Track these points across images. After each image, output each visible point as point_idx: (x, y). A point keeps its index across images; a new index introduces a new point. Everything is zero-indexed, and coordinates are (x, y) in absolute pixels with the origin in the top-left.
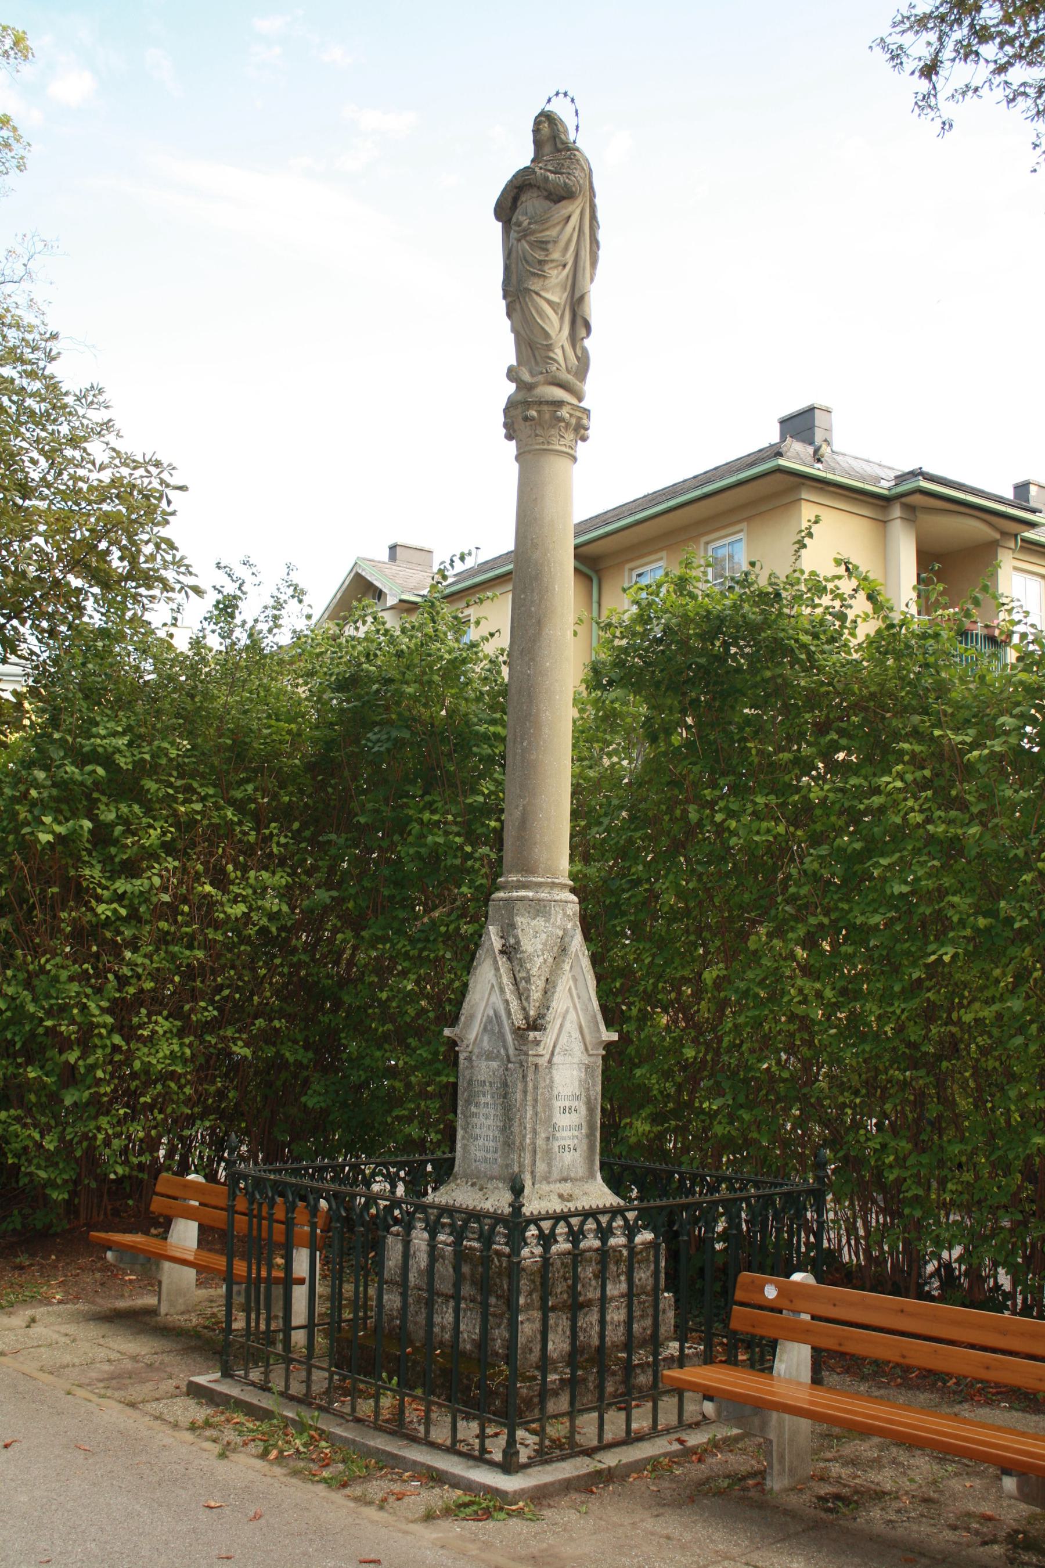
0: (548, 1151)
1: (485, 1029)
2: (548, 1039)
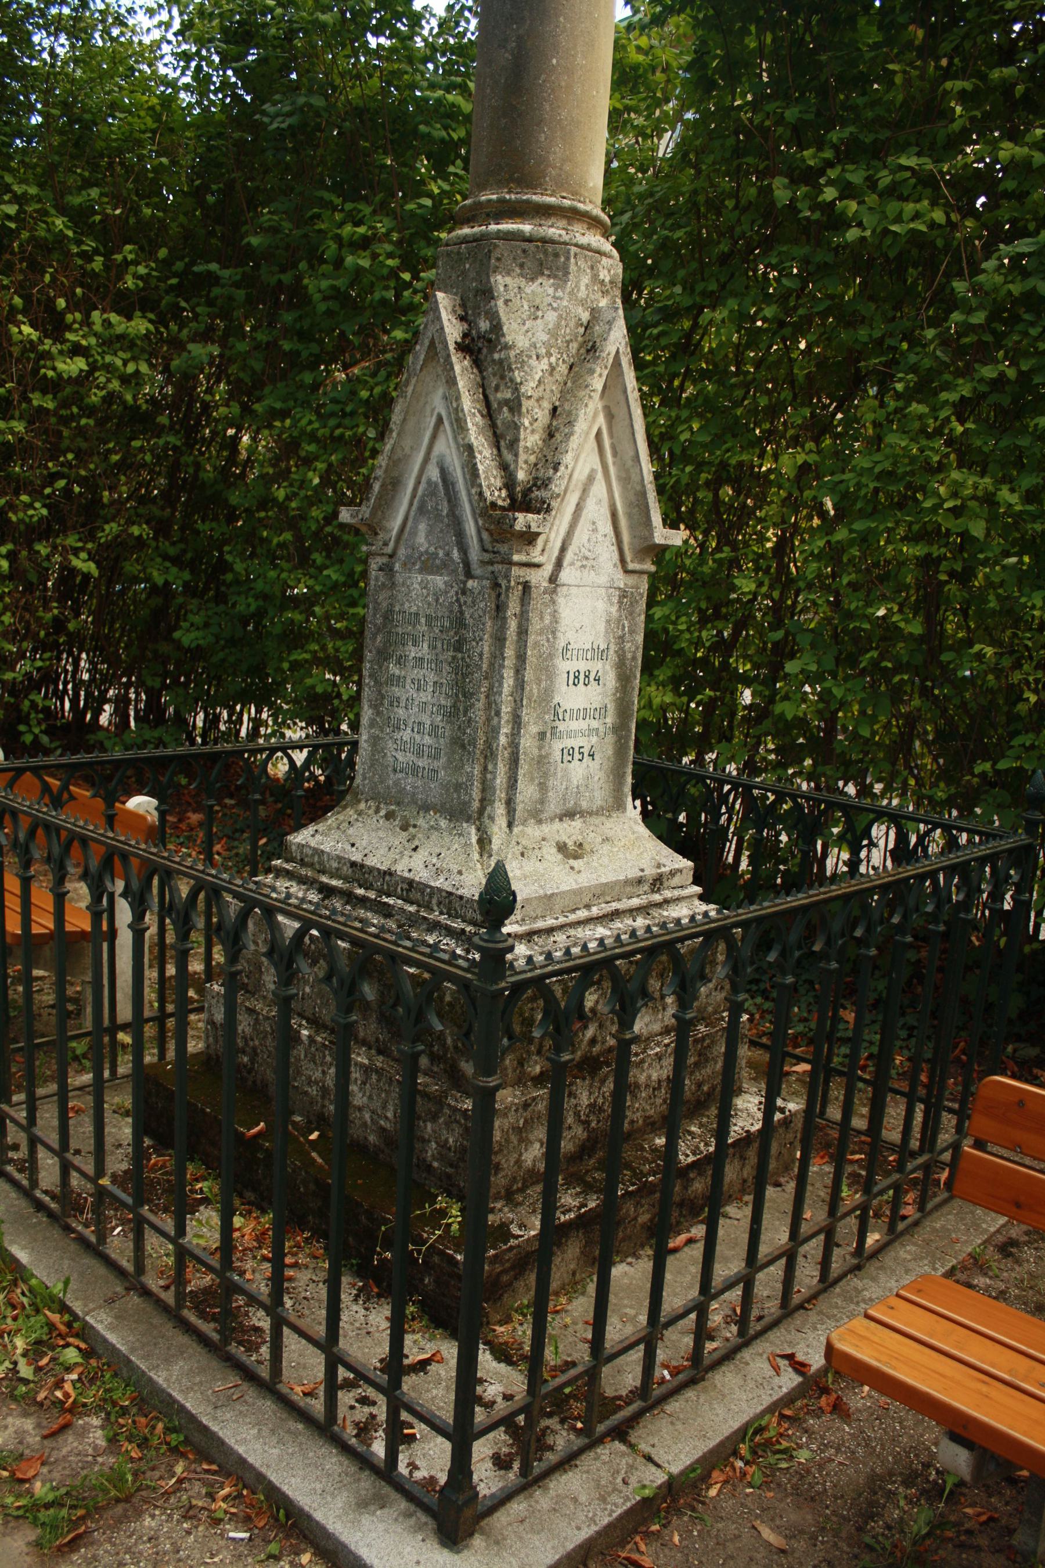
0: (542, 761)
1: (422, 510)
2: (553, 531)
